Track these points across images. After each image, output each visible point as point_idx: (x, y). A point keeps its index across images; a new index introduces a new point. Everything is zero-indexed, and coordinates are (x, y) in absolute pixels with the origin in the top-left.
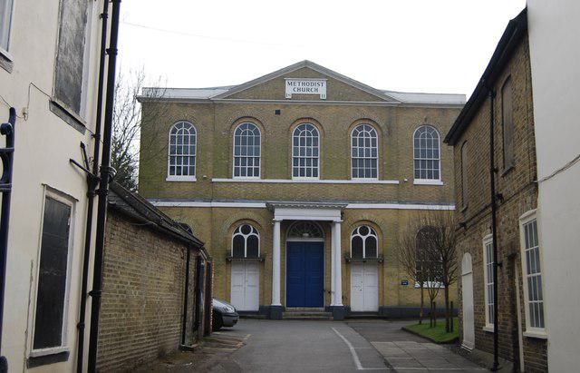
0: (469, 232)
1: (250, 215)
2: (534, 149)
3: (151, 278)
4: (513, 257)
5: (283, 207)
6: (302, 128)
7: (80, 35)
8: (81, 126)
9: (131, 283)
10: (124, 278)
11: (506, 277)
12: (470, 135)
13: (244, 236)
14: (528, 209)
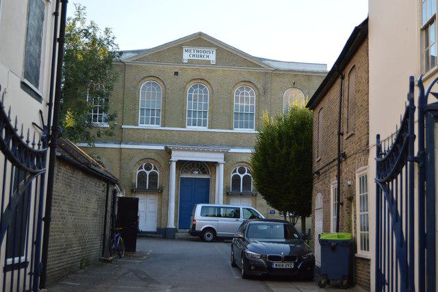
0: (321, 178)
1: (152, 155)
2: (368, 123)
3: (82, 207)
4: (351, 199)
5: (178, 150)
6: (195, 87)
7: (40, 30)
8: (38, 98)
9: (69, 211)
10: (65, 207)
11: (346, 213)
12: (325, 103)
13: (151, 171)
14: (361, 166)
